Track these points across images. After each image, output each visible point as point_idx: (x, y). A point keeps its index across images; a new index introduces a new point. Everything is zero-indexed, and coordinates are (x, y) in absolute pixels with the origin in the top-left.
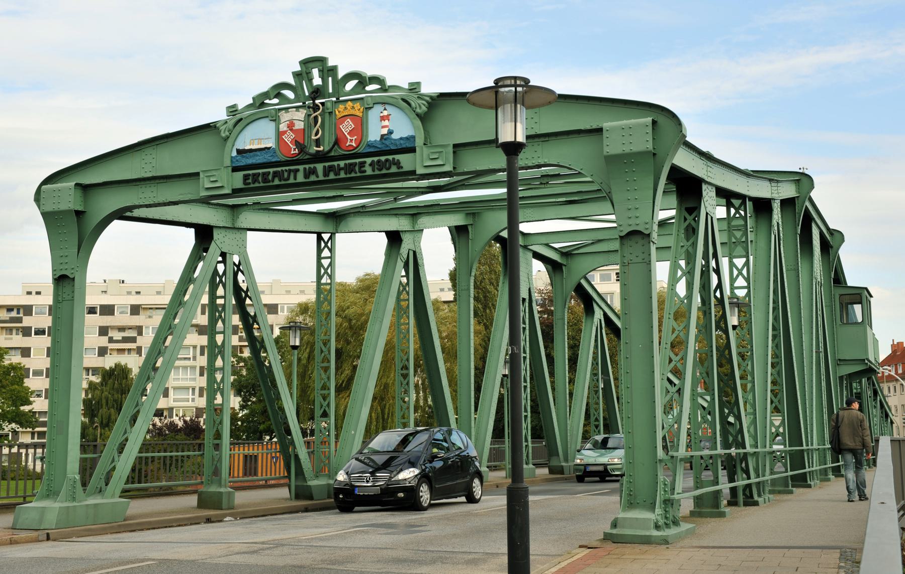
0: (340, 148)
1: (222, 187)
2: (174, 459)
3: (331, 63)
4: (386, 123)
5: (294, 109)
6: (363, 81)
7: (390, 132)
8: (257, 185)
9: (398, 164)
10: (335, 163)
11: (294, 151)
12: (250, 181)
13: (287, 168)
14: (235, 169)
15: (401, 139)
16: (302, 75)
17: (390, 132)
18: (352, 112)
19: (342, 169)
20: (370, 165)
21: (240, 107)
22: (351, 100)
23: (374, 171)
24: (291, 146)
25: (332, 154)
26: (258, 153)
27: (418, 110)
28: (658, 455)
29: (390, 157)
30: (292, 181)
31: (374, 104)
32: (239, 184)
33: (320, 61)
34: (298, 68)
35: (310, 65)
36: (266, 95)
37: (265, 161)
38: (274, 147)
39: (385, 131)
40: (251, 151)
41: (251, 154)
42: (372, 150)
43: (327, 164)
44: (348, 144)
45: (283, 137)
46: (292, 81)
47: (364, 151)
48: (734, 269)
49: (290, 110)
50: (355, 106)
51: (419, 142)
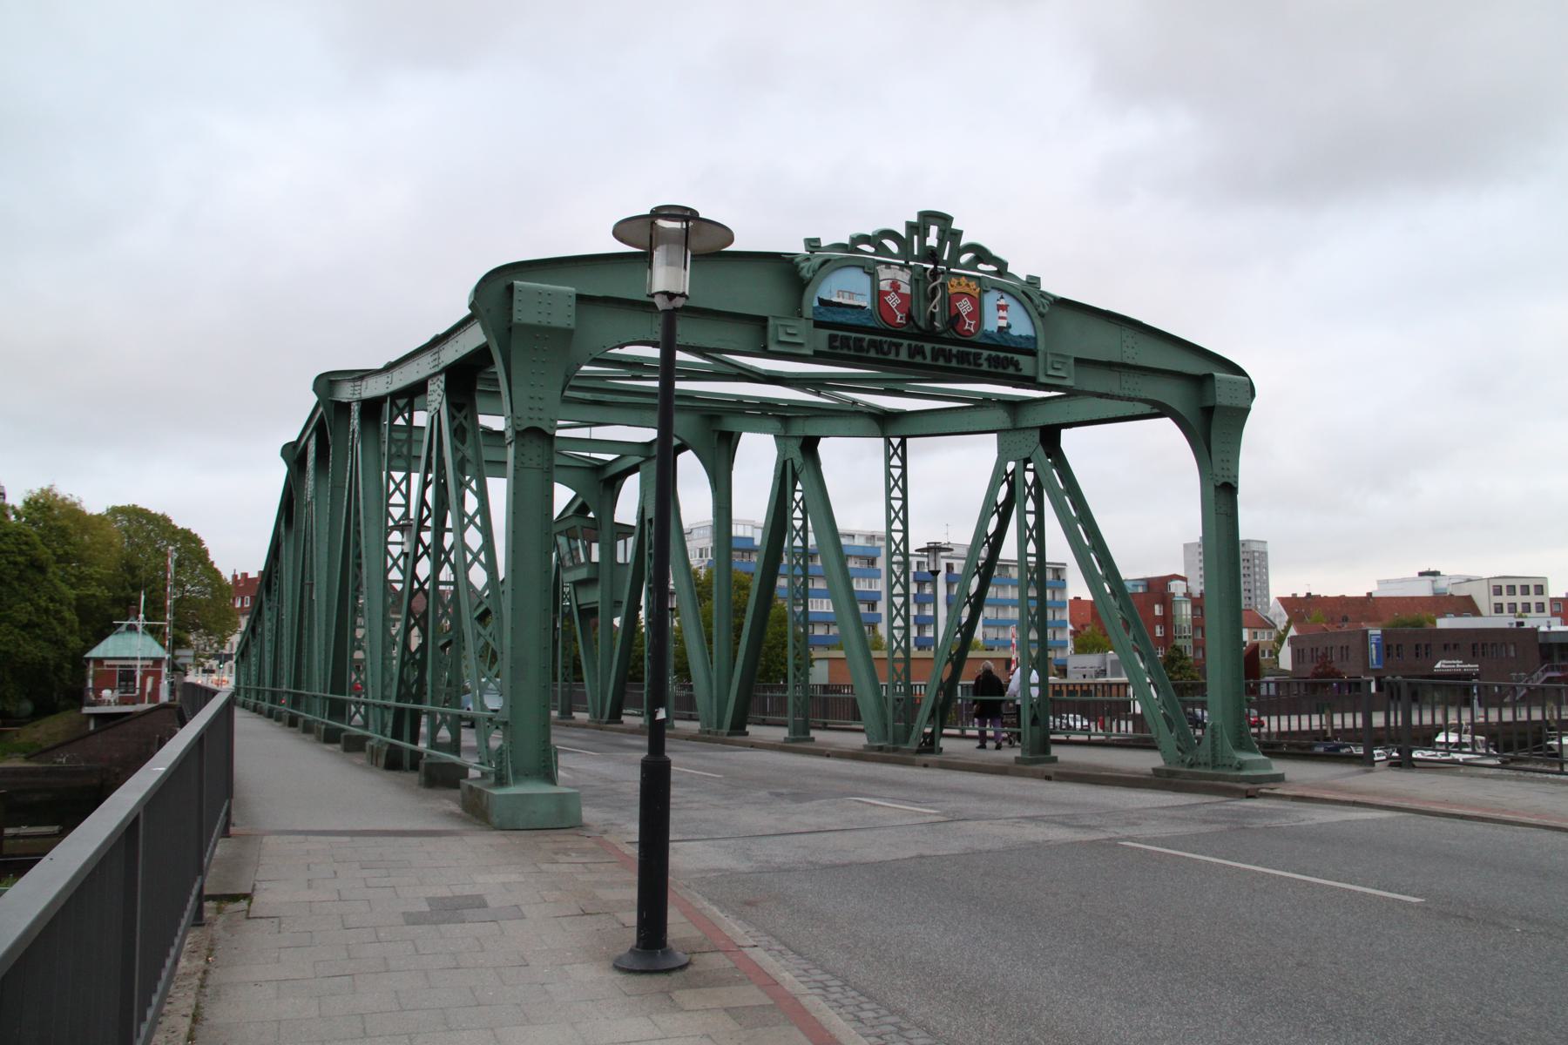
0: (955, 330)
1: (801, 345)
2: (838, 716)
3: (955, 226)
4: (1002, 313)
5: (898, 267)
6: (981, 254)
7: (1009, 326)
8: (845, 351)
9: (1016, 365)
10: (947, 347)
11: (900, 318)
12: (837, 344)
13: (889, 339)
14: (819, 325)
15: (1020, 336)
16: (919, 227)
17: (1009, 326)
18: (967, 290)
19: (955, 356)
20: (986, 359)
21: (824, 243)
22: (966, 276)
23: (990, 366)
24: (898, 313)
25: (945, 335)
26: (849, 311)
27: (1041, 309)
28: (392, 716)
29: (1009, 355)
30: (892, 357)
31: (993, 288)
32: (824, 347)
33: (943, 220)
34: (914, 219)
35: (930, 220)
36: (865, 239)
37: (858, 323)
38: (869, 307)
39: (1003, 323)
40: (839, 305)
41: (841, 309)
42: (989, 341)
43: (937, 346)
44: (966, 327)
45: (887, 299)
46: (903, 232)
47: (981, 341)
48: (404, 491)
49: (892, 266)
50: (971, 284)
51: (1041, 346)
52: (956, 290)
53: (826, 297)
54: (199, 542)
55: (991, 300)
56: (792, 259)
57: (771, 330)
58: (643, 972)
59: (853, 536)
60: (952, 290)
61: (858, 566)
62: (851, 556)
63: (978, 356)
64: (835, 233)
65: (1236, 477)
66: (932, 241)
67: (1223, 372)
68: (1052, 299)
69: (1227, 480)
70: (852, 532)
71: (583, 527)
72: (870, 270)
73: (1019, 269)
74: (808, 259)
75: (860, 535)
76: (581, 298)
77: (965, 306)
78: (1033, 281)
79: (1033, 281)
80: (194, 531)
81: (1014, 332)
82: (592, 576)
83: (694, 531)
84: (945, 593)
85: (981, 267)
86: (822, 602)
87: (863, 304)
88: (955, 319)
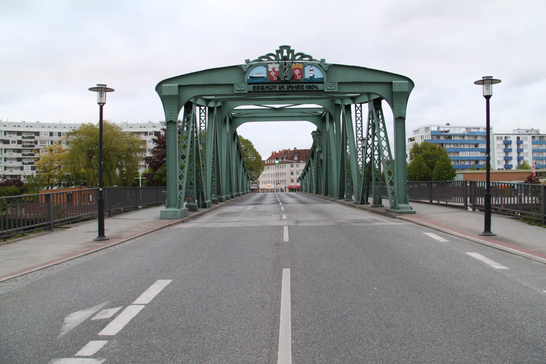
3: (291, 49)
6: (303, 56)
7: (314, 76)
8: (258, 90)
9: (316, 87)
10: (292, 85)
11: (275, 78)
13: (272, 85)
14: (249, 84)
15: (318, 78)
17: (314, 76)
21: (251, 61)
22: (298, 63)
23: (307, 89)
26: (259, 78)
27: (325, 69)
29: (314, 85)
30: (274, 90)
31: (308, 65)
33: (288, 47)
34: (278, 49)
36: (263, 57)
37: (262, 81)
38: (266, 76)
39: (312, 75)
40: (256, 77)
41: (256, 78)
43: (288, 85)
46: (275, 53)
51: (325, 80)
52: (295, 67)
53: (252, 76)
54: (251, 143)
55: (307, 69)
56: (241, 67)
57: (235, 87)
58: (99, 240)
59: (479, 128)
60: (293, 68)
61: (481, 139)
62: (478, 136)
63: (303, 86)
64: (253, 57)
65: (405, 115)
66: (285, 53)
67: (405, 81)
68: (329, 65)
69: (400, 116)
70: (478, 127)
71: (317, 135)
72: (266, 66)
73: (317, 57)
74: (245, 66)
75: (482, 128)
76: (179, 86)
77: (297, 72)
78: (323, 61)
79: (323, 61)
80: (249, 140)
81: (315, 77)
82: (320, 150)
83: (420, 130)
84: (516, 148)
85: (304, 59)
86: (467, 153)
87: (264, 76)
88: (294, 76)
